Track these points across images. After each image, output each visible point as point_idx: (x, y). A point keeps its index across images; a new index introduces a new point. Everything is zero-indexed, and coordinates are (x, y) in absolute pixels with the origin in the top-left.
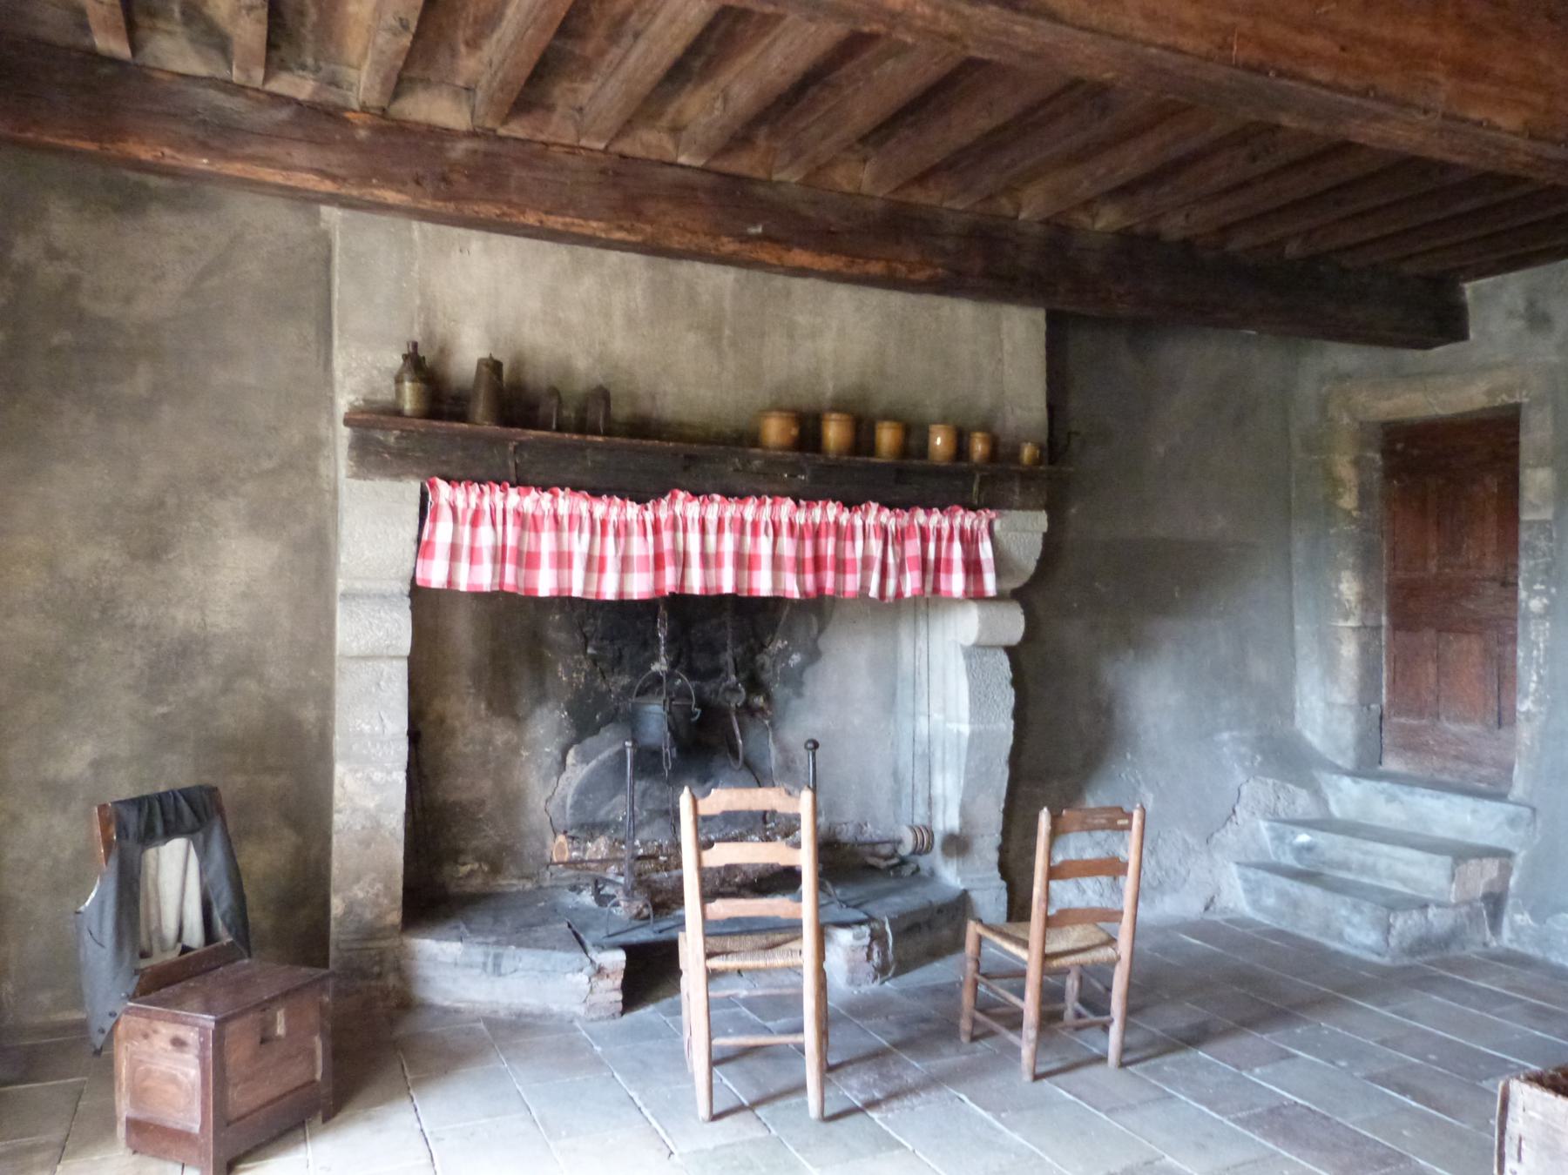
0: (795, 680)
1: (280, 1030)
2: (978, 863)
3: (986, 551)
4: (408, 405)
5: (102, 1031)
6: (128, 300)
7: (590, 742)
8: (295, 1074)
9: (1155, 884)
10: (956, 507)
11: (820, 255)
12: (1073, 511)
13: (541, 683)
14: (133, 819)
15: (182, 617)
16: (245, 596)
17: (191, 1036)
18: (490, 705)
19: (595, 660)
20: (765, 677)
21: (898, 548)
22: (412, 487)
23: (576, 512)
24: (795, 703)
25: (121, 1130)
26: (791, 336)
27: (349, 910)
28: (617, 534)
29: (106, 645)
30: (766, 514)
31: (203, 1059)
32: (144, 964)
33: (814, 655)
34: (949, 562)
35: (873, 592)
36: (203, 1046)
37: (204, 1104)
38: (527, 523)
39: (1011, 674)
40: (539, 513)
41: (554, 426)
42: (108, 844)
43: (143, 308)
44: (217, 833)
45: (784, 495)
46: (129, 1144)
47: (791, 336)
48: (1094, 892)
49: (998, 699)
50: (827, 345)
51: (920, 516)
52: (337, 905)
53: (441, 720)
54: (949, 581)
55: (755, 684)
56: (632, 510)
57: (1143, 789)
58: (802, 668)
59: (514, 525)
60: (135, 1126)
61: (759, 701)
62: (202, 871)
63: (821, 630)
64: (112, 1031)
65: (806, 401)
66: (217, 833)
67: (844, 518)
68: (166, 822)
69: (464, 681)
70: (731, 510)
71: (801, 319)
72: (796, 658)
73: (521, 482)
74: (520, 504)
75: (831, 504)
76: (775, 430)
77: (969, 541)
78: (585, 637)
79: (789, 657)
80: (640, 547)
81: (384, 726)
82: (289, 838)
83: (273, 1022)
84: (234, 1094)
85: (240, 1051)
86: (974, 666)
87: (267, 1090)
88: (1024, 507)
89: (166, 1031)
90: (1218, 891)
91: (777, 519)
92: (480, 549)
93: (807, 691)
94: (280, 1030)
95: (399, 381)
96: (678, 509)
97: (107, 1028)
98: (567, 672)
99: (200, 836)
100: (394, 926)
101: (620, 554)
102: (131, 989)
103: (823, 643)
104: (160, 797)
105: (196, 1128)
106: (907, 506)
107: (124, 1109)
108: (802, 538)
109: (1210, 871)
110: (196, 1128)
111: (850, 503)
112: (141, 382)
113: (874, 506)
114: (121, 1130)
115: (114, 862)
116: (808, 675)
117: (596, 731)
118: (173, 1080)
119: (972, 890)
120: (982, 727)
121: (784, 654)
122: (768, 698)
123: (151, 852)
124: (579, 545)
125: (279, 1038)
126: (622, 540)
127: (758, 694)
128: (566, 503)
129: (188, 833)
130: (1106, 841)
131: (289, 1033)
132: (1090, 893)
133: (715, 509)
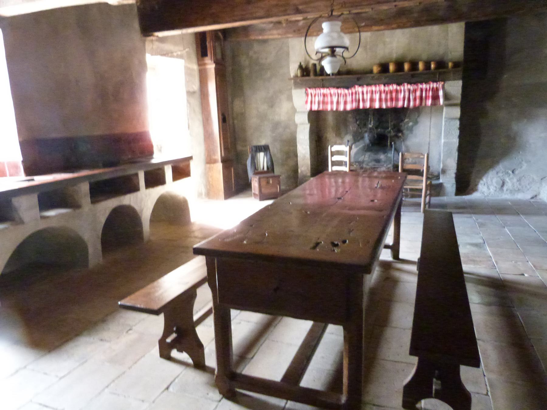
0: (411, 130)
1: (271, 182)
2: (448, 177)
3: (441, 93)
4: (299, 75)
6: (266, 59)
7: (357, 143)
8: (273, 190)
9: (517, 189)
10: (430, 82)
11: (380, 26)
12: (505, 76)
13: (347, 130)
14: (254, 149)
15: (277, 118)
18: (336, 135)
19: (358, 125)
20: (402, 128)
21: (414, 94)
22: (304, 90)
23: (335, 92)
24: (410, 135)
26: (384, 44)
28: (343, 96)
30: (378, 88)
33: (416, 123)
34: (429, 97)
35: (405, 106)
38: (324, 95)
39: (459, 126)
40: (327, 93)
41: (325, 75)
43: (269, 61)
44: (268, 152)
45: (381, 84)
47: (384, 44)
48: (493, 189)
49: (453, 133)
50: (395, 45)
51: (420, 86)
52: (299, 171)
53: (326, 138)
54: (428, 102)
55: (399, 131)
56: (346, 91)
57: (523, 163)
58: (412, 126)
61: (400, 134)
63: (418, 116)
65: (383, 61)
66: (268, 152)
67: (398, 88)
68: (259, 150)
69: (331, 130)
70: (369, 88)
71: (387, 40)
72: (411, 124)
73: (323, 87)
74: (323, 92)
75: (394, 85)
76: (376, 69)
77: (435, 91)
78: (357, 120)
79: (409, 123)
80: (349, 99)
81: (305, 138)
85: (264, 183)
86: (447, 124)
88: (454, 79)
90: (539, 193)
91: (381, 90)
92: (382, 99)
93: (414, 132)
94: (271, 182)
95: (298, 70)
96: (357, 89)
98: (352, 127)
100: (309, 176)
101: (344, 100)
102: (253, 173)
103: (418, 120)
104: (259, 146)
106: (416, 83)
107: (253, 191)
108: (387, 94)
109: (538, 188)
111: (399, 84)
112: (269, 74)
113: (406, 84)
116: (414, 128)
117: (359, 141)
119: (445, 183)
120: (447, 140)
121: (408, 123)
122: (403, 134)
124: (335, 99)
126: (344, 98)
127: (400, 133)
128: (333, 91)
129: (264, 152)
130: (502, 176)
131: (272, 182)
132: (491, 190)
133: (365, 89)
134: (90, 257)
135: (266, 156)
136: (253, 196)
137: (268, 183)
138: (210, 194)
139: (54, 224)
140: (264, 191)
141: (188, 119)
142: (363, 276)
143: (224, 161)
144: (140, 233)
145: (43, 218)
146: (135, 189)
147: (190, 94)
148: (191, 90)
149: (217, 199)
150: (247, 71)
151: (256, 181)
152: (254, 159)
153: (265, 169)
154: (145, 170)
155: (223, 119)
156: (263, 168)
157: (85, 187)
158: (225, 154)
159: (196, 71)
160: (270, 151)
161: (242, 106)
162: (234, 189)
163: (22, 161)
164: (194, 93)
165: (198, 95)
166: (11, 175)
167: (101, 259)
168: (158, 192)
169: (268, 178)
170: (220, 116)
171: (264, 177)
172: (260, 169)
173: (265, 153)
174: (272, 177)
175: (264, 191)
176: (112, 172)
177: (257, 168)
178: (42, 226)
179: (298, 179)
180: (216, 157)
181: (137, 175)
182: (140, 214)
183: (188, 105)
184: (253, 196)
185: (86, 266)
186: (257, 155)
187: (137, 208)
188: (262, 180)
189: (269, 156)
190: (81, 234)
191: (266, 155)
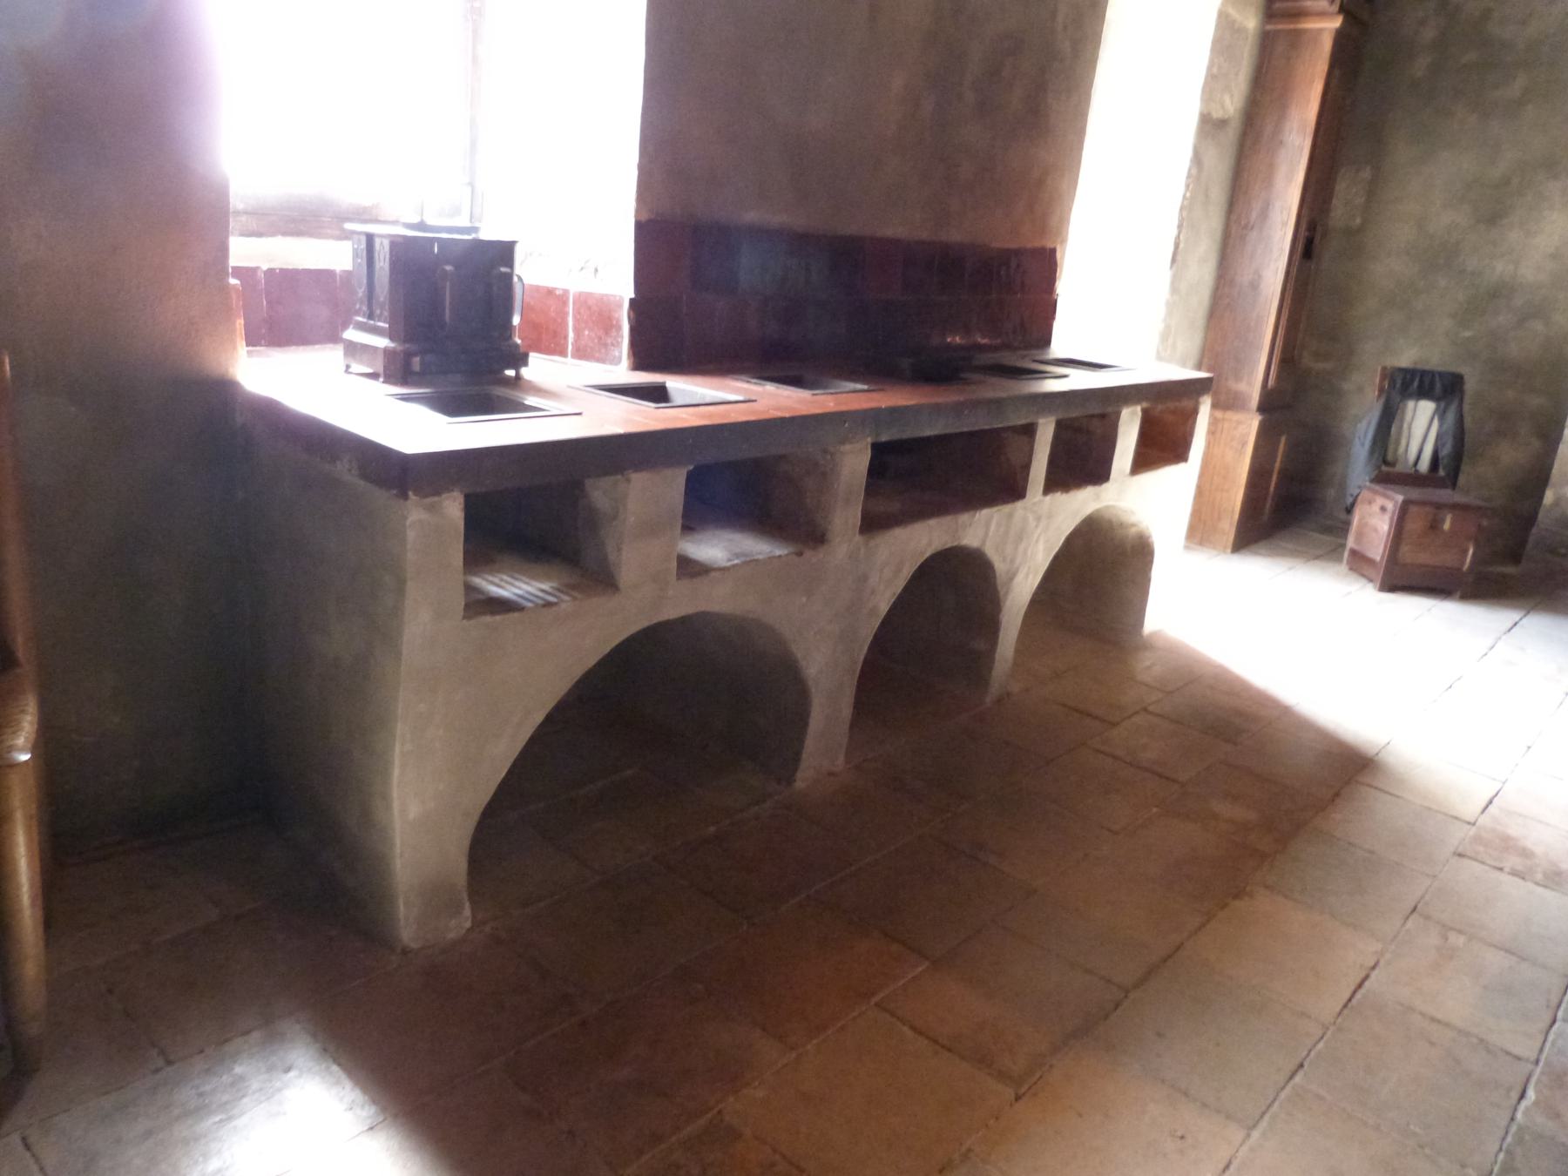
1: (1447, 526)
5: (1352, 495)
8: (1447, 559)
15: (1500, 268)
16: (1554, 256)
17: (1390, 506)
25: (1346, 554)
27: (1557, 503)
29: (1443, 283)
31: (1392, 519)
32: (1384, 468)
36: (1394, 513)
37: (1385, 546)
42: (1381, 390)
46: (1348, 563)
59: (1255, 286)
60: (1354, 553)
62: (1441, 426)
64: (1358, 495)
68: (1421, 386)
82: (1536, 444)
83: (1443, 521)
84: (1405, 549)
85: (1415, 525)
87: (1424, 558)
89: (1380, 501)
97: (1355, 494)
99: (1443, 405)
102: (1373, 477)
105: (1378, 558)
107: (1351, 542)
110: (1378, 558)
114: (1346, 554)
115: (1382, 400)
118: (1376, 530)
123: (1411, 404)
125: (1443, 531)
134: (811, 744)
135: (1442, 419)
136: (338, 278)
137: (1434, 526)
138: (1199, 532)
139: (716, 600)
140: (1407, 554)
141: (1180, 227)
142: (239, 272)
143: (1270, 405)
144: (977, 664)
145: (689, 568)
146: (1011, 489)
147: (1210, 125)
148: (1217, 114)
149: (1149, 537)
150: (1420, 67)
151: (1383, 509)
152: (1389, 419)
153: (1424, 465)
154: (1061, 417)
155: (1307, 246)
156: (1418, 458)
157: (854, 462)
158: (1279, 377)
159: (1250, 39)
160: (1461, 400)
161: (1360, 201)
162: (1265, 518)
163: (632, 301)
164: (1222, 123)
165: (1231, 134)
166: (582, 353)
167: (841, 760)
168: (1081, 503)
169: (1439, 506)
170: (1304, 226)
171: (1423, 503)
172: (1406, 459)
173: (1443, 405)
174: (1454, 507)
175: (1407, 554)
176: (958, 409)
177: (1390, 457)
178: (679, 603)
179: (1534, 530)
180: (1242, 386)
181: (1029, 431)
182: (1002, 593)
183: (1194, 171)
184: (338, 278)
185: (790, 780)
186: (1405, 405)
187: (1000, 566)
188: (1413, 509)
189: (1451, 417)
190: (798, 651)
191: (1441, 413)
